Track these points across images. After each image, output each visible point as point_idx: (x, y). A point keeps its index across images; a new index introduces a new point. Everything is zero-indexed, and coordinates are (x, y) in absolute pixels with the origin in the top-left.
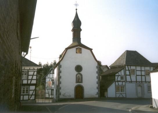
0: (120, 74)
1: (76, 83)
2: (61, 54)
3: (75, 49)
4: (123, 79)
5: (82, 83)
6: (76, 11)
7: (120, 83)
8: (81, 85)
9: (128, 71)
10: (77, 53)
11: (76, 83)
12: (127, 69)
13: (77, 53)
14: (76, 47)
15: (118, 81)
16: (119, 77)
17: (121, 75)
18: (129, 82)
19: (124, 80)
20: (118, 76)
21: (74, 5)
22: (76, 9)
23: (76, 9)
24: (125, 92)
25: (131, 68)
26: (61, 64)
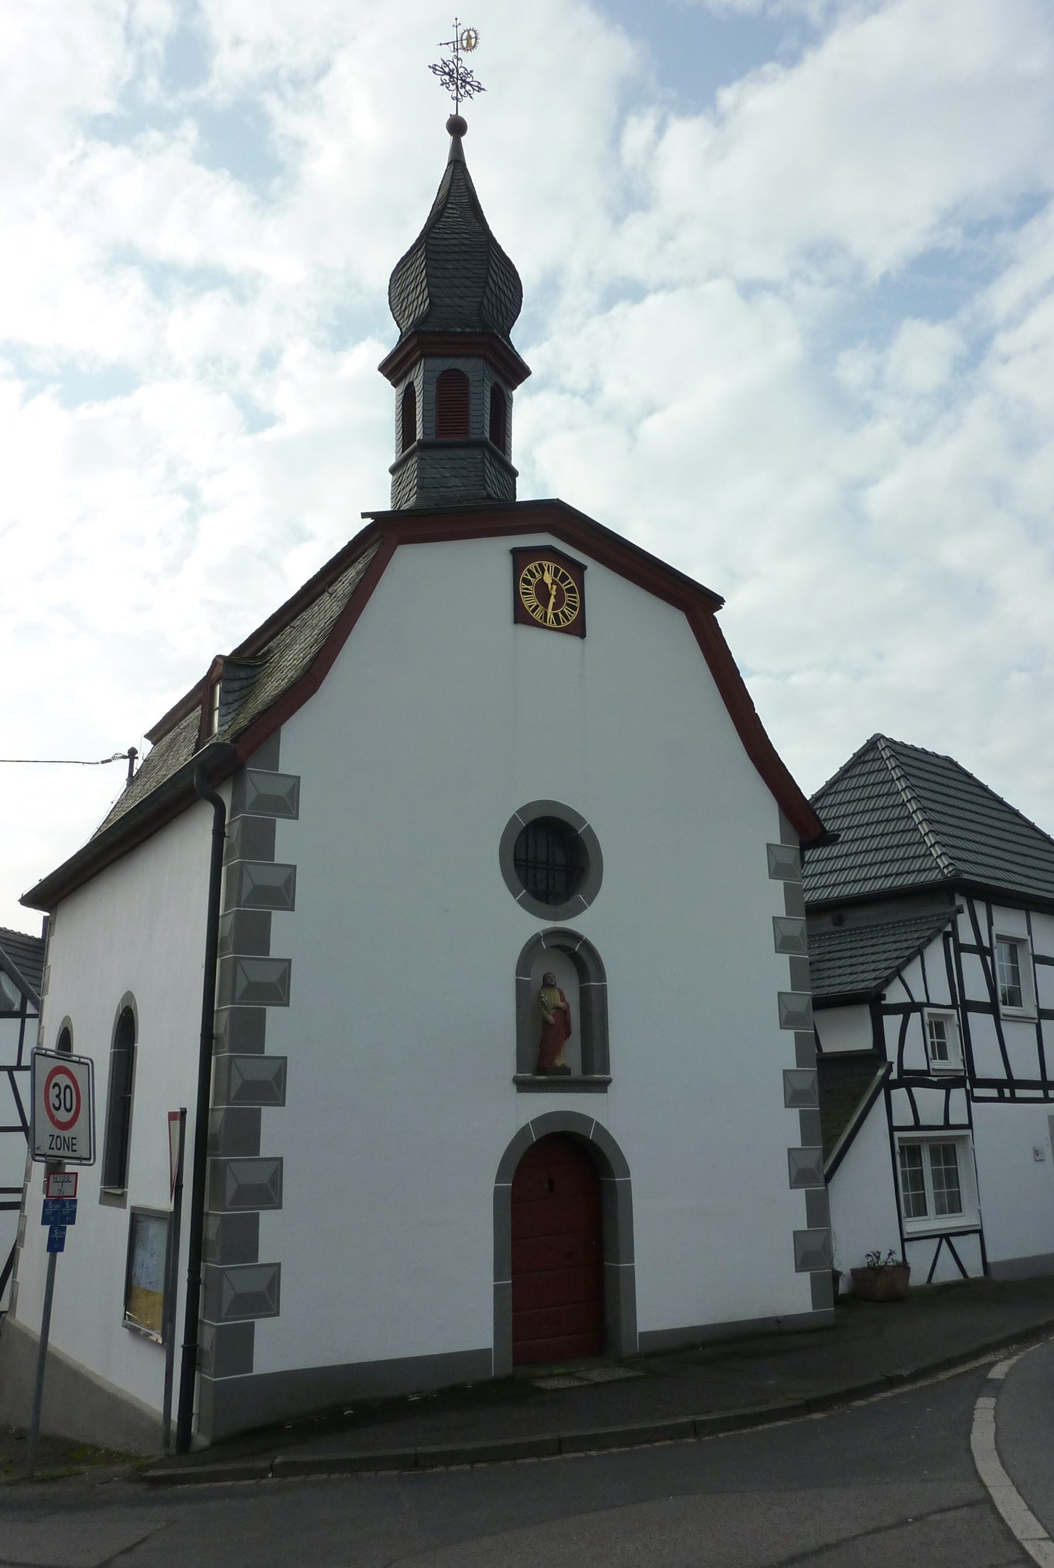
0: (920, 997)
1: (522, 1085)
2: (993, 927)
3: (506, 565)
4: (943, 1056)
5: (602, 1086)
6: (448, 139)
7: (930, 1100)
8: (587, 1120)
9: (977, 958)
10: (521, 616)
11: (522, 1085)
12: (966, 936)
13: (521, 616)
14: (268, 959)
15: (913, 1080)
16: (915, 1017)
17: (929, 1005)
18: (993, 1093)
19: (955, 1062)
20: (906, 1009)
21: (434, 68)
22: (457, 127)
23: (440, 46)
24: (897, 1135)
25: (997, 929)
26: (286, 765)
